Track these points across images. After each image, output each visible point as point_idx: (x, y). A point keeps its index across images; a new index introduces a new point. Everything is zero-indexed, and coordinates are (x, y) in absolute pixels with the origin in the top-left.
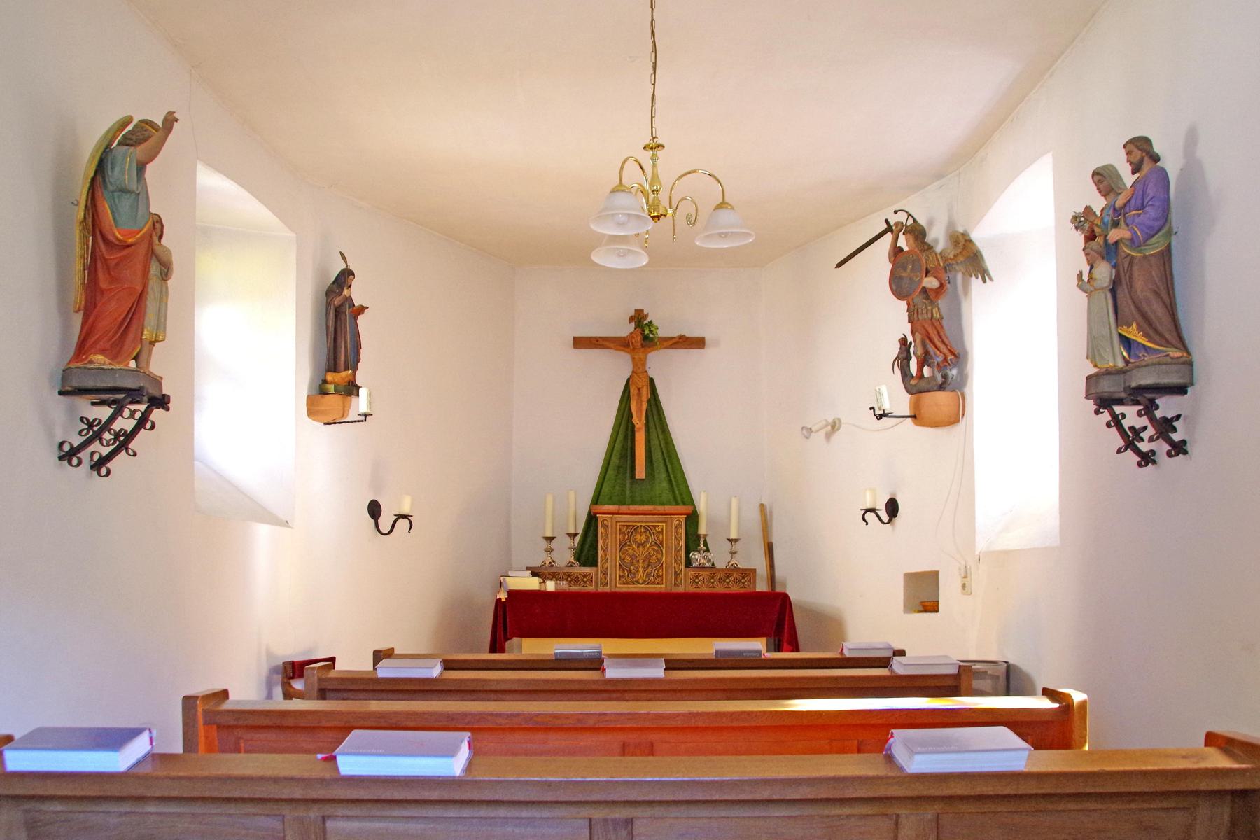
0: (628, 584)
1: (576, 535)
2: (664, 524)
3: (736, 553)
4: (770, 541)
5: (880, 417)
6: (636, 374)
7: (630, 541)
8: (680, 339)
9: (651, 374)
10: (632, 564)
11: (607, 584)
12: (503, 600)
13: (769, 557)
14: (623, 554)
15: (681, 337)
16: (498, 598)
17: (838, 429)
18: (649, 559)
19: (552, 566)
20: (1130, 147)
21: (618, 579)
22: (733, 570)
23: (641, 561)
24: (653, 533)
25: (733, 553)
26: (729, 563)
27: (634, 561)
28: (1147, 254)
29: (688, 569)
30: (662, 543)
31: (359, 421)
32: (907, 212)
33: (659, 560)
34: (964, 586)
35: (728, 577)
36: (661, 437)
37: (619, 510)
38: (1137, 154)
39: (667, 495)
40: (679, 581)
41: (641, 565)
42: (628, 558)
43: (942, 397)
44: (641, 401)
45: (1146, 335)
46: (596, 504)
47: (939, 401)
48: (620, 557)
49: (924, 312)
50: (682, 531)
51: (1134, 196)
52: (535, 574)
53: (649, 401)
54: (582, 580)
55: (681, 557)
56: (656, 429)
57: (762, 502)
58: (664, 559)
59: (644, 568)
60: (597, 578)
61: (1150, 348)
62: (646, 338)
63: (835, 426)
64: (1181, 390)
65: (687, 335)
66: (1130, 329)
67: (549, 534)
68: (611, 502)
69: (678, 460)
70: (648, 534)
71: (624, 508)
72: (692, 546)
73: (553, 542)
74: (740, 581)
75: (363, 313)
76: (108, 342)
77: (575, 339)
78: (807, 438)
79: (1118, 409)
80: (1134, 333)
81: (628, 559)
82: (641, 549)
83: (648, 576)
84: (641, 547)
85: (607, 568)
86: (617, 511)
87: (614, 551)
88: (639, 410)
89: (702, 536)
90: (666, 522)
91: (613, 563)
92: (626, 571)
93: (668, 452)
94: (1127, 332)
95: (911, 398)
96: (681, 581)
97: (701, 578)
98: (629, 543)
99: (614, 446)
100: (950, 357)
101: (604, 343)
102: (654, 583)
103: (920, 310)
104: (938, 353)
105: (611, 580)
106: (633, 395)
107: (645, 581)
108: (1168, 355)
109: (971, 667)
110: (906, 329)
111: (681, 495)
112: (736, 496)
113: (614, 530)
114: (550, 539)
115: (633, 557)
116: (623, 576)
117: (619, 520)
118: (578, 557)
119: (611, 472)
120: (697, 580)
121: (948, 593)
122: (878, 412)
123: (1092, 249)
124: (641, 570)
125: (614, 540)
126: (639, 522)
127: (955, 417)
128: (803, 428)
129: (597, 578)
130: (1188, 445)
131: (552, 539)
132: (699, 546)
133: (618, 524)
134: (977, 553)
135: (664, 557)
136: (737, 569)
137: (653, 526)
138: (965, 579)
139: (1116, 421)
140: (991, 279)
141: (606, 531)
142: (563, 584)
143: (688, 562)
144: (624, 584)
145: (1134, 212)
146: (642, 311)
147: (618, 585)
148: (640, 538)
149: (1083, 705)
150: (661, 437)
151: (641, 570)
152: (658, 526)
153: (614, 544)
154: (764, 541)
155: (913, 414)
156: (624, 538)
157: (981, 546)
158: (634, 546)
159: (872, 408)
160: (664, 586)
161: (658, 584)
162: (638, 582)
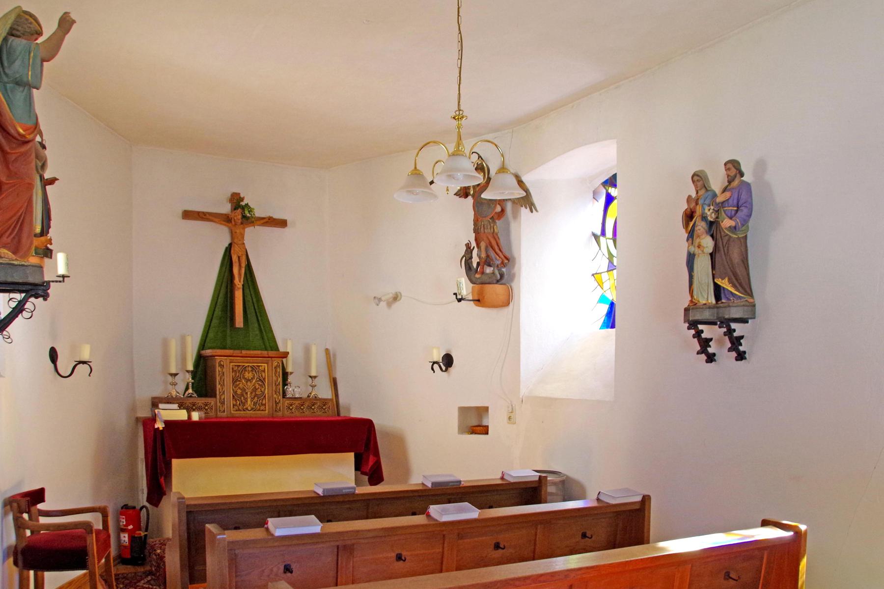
0: (239, 410)
2: (266, 365)
5: (459, 300)
7: (240, 378)
8: (269, 219)
10: (242, 395)
11: (224, 411)
13: (335, 389)
14: (235, 387)
15: (270, 218)
17: (399, 301)
18: (255, 392)
20: (730, 166)
21: (232, 407)
25: (313, 386)
26: (310, 393)
28: (740, 236)
29: (284, 399)
31: (57, 281)
32: (478, 154)
33: (263, 393)
34: (510, 418)
35: (313, 405)
37: (233, 353)
38: (733, 172)
40: (278, 408)
43: (499, 289)
45: (734, 286)
47: (495, 291)
48: (233, 390)
49: (489, 227)
51: (732, 198)
52: (181, 406)
54: (205, 408)
55: (279, 389)
56: (249, 288)
57: (327, 347)
58: (266, 392)
59: (252, 398)
61: (741, 296)
62: (244, 217)
63: (396, 298)
64: (744, 321)
66: (723, 281)
70: (254, 372)
74: (311, 408)
75: (53, 184)
76: (7, 238)
78: (378, 305)
79: (701, 327)
80: (724, 284)
83: (255, 404)
85: (224, 399)
86: (231, 354)
88: (240, 274)
89: (289, 373)
90: (267, 363)
94: (721, 283)
95: (473, 287)
96: (280, 408)
99: (218, 299)
100: (506, 261)
101: (211, 218)
102: (259, 410)
103: (486, 226)
104: (498, 258)
107: (252, 409)
108: (746, 301)
109: (546, 477)
110: (472, 237)
112: (315, 344)
116: (236, 405)
120: (291, 407)
121: (493, 421)
122: (459, 297)
123: (702, 227)
124: (249, 400)
126: (247, 363)
127: (507, 301)
128: (375, 297)
130: (747, 354)
133: (231, 364)
134: (521, 397)
135: (266, 390)
137: (257, 366)
138: (511, 414)
139: (698, 334)
140: (536, 210)
144: (236, 411)
145: (731, 208)
146: (239, 194)
148: (248, 375)
149: (806, 531)
152: (261, 366)
154: (330, 377)
155: (476, 298)
156: (236, 375)
157: (524, 391)
158: (243, 381)
159: (455, 294)
161: (262, 410)
162: (247, 409)
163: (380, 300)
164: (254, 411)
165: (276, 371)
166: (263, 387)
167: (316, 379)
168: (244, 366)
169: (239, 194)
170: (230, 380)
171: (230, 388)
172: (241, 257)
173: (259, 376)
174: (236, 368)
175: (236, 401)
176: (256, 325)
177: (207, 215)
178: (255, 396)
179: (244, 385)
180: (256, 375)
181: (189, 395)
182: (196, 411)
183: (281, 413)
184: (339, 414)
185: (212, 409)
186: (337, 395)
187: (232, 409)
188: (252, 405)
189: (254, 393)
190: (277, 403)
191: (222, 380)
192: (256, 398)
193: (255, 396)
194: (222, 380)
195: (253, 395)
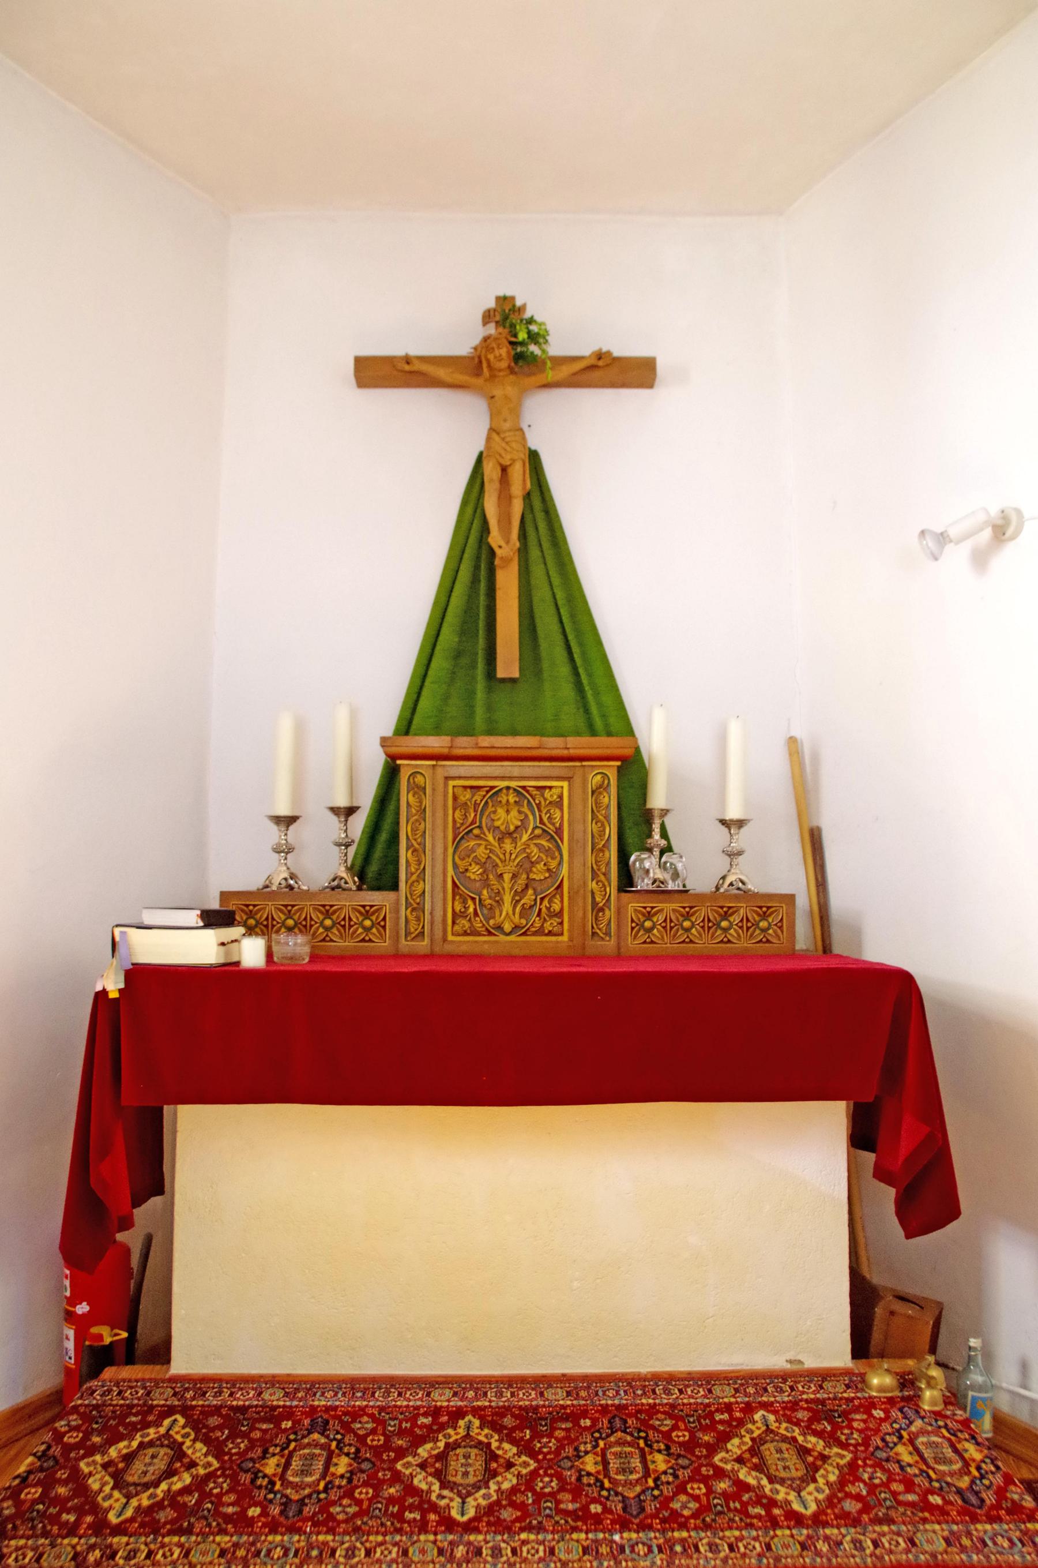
0: (474, 933)
1: (350, 811)
2: (565, 784)
3: (740, 853)
4: (814, 824)
6: (498, 434)
7: (480, 827)
8: (600, 359)
9: (533, 443)
10: (486, 883)
11: (422, 933)
12: (113, 995)
16: (99, 988)
17: (1013, 538)
19: (291, 888)
22: (736, 896)
23: (507, 877)
24: (539, 806)
25: (733, 855)
26: (724, 878)
27: (491, 877)
29: (623, 895)
30: (559, 831)
35: (725, 916)
36: (556, 581)
39: (571, 715)
41: (507, 885)
42: (475, 868)
44: (510, 498)
46: (407, 733)
48: (455, 866)
50: (610, 799)
52: (212, 919)
53: (527, 496)
54: (361, 924)
55: (608, 864)
58: (565, 871)
60: (398, 918)
65: (616, 353)
67: (284, 810)
68: (437, 730)
69: (599, 643)
70: (525, 809)
71: (464, 744)
72: (631, 839)
73: (291, 828)
77: (361, 363)
81: (474, 873)
82: (508, 845)
83: (525, 912)
84: (508, 841)
86: (445, 751)
87: (439, 850)
89: (656, 813)
90: (569, 779)
91: (439, 880)
92: (470, 902)
93: (573, 616)
97: (659, 918)
98: (476, 832)
102: (540, 932)
105: (432, 923)
106: (491, 480)
107: (516, 927)
111: (604, 716)
113: (440, 798)
114: (287, 821)
115: (488, 866)
116: (463, 915)
117: (453, 772)
118: (360, 872)
119: (439, 663)
124: (507, 898)
125: (439, 822)
126: (503, 778)
128: (923, 532)
129: (397, 919)
131: (290, 820)
132: (650, 835)
133: (451, 783)
135: (565, 865)
136: (746, 895)
141: (421, 802)
142: (295, 944)
143: (626, 879)
144: (465, 933)
146: (513, 298)
147: (450, 938)
148: (506, 818)
150: (556, 581)
151: (507, 898)
152: (550, 788)
153: (440, 834)
158: (490, 838)
160: (565, 938)
162: (499, 928)
163: (942, 539)
164: (524, 934)
165: (598, 803)
166: (553, 858)
167: (743, 830)
168: (492, 788)
169: (513, 298)
170: (445, 837)
171: (445, 861)
172: (510, 470)
173: (541, 821)
174: (465, 796)
175: (464, 902)
176: (565, 670)
177: (416, 362)
178: (527, 886)
179: (491, 851)
180: (531, 817)
181: (336, 883)
182: (257, 934)
183: (426, 941)
184: (826, 948)
185: (384, 927)
186: (821, 884)
187: (449, 928)
188: (517, 916)
189: (524, 876)
190: (598, 910)
191: (419, 833)
192: (530, 891)
193: (527, 886)
194: (419, 833)
195: (520, 882)
